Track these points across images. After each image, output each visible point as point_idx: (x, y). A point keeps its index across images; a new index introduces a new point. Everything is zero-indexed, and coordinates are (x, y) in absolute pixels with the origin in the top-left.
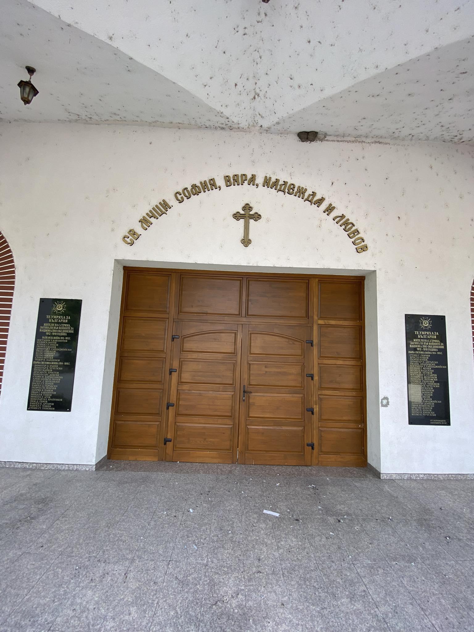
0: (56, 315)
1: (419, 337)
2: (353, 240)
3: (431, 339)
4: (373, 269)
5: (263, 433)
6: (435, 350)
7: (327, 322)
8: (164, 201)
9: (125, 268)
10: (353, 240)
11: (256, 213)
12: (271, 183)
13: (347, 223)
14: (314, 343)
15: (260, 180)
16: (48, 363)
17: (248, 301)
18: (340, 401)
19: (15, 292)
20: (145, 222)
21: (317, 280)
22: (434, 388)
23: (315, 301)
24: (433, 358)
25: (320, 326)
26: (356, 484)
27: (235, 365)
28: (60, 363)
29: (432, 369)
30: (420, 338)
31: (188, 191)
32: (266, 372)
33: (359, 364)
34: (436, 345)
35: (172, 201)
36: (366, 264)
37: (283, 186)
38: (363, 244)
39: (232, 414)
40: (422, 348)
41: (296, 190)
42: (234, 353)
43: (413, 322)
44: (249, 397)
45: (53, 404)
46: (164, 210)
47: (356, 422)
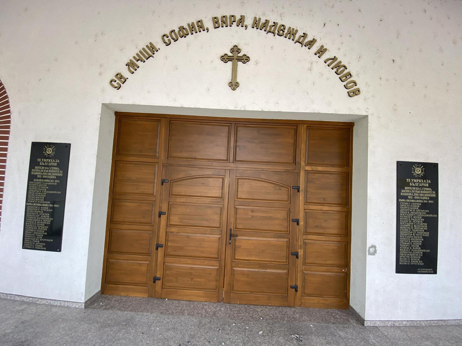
0: (416, 178)
1: (411, 185)
2: (345, 83)
3: (423, 187)
4: (365, 114)
5: (248, 275)
6: (426, 198)
7: (314, 168)
8: (151, 43)
9: (117, 114)
10: (345, 83)
11: (245, 55)
12: (261, 24)
13: (338, 66)
14: (301, 189)
15: (249, 21)
16: (39, 205)
17: (235, 147)
18: (323, 245)
19: (11, 136)
20: (132, 66)
21: (305, 126)
22: (423, 237)
23: (303, 147)
24: (424, 206)
25: (307, 172)
26: (341, 334)
27: (221, 209)
28: (50, 205)
29: (423, 218)
30: (412, 186)
31: (175, 34)
32: (252, 216)
33: (345, 210)
34: (428, 193)
35: (159, 44)
36: (358, 109)
37: (273, 27)
38: (355, 87)
39: (218, 255)
40: (413, 196)
41: (286, 31)
42: (222, 198)
43: (405, 170)
44: (235, 239)
45: (44, 244)
46: (150, 53)
47: (339, 266)
